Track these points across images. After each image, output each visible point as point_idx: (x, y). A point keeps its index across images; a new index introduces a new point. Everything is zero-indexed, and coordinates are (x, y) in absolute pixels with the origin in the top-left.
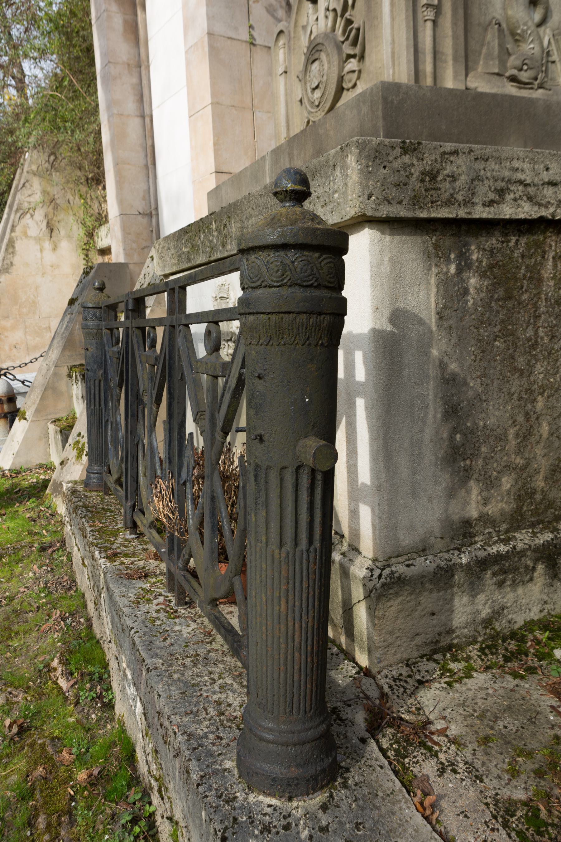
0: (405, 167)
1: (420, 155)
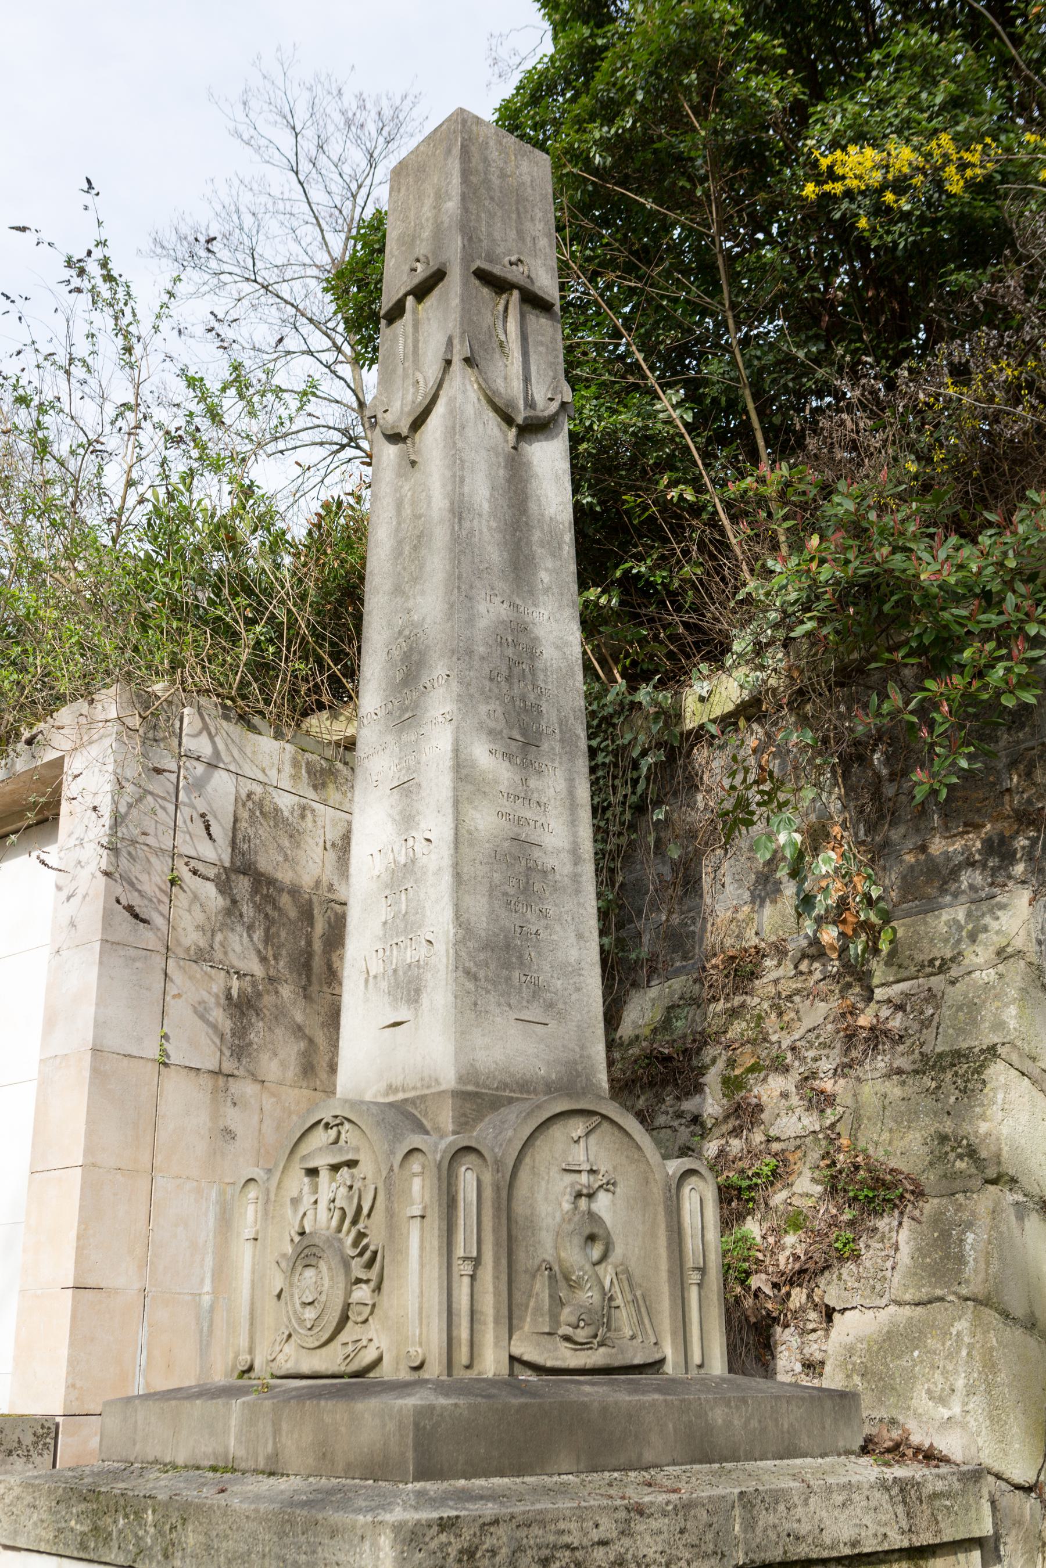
0: (442, 1547)
1: (458, 1531)
